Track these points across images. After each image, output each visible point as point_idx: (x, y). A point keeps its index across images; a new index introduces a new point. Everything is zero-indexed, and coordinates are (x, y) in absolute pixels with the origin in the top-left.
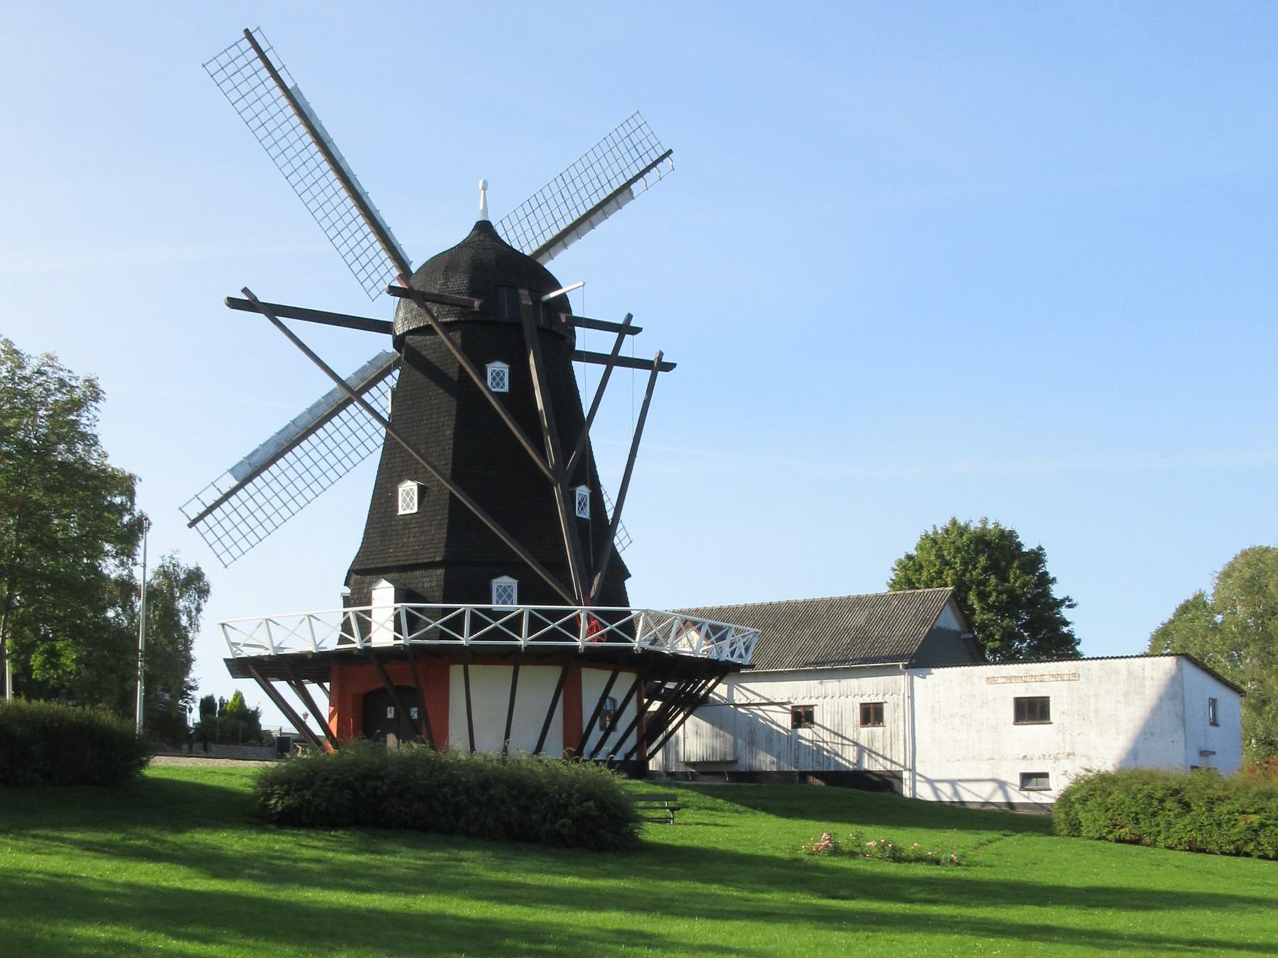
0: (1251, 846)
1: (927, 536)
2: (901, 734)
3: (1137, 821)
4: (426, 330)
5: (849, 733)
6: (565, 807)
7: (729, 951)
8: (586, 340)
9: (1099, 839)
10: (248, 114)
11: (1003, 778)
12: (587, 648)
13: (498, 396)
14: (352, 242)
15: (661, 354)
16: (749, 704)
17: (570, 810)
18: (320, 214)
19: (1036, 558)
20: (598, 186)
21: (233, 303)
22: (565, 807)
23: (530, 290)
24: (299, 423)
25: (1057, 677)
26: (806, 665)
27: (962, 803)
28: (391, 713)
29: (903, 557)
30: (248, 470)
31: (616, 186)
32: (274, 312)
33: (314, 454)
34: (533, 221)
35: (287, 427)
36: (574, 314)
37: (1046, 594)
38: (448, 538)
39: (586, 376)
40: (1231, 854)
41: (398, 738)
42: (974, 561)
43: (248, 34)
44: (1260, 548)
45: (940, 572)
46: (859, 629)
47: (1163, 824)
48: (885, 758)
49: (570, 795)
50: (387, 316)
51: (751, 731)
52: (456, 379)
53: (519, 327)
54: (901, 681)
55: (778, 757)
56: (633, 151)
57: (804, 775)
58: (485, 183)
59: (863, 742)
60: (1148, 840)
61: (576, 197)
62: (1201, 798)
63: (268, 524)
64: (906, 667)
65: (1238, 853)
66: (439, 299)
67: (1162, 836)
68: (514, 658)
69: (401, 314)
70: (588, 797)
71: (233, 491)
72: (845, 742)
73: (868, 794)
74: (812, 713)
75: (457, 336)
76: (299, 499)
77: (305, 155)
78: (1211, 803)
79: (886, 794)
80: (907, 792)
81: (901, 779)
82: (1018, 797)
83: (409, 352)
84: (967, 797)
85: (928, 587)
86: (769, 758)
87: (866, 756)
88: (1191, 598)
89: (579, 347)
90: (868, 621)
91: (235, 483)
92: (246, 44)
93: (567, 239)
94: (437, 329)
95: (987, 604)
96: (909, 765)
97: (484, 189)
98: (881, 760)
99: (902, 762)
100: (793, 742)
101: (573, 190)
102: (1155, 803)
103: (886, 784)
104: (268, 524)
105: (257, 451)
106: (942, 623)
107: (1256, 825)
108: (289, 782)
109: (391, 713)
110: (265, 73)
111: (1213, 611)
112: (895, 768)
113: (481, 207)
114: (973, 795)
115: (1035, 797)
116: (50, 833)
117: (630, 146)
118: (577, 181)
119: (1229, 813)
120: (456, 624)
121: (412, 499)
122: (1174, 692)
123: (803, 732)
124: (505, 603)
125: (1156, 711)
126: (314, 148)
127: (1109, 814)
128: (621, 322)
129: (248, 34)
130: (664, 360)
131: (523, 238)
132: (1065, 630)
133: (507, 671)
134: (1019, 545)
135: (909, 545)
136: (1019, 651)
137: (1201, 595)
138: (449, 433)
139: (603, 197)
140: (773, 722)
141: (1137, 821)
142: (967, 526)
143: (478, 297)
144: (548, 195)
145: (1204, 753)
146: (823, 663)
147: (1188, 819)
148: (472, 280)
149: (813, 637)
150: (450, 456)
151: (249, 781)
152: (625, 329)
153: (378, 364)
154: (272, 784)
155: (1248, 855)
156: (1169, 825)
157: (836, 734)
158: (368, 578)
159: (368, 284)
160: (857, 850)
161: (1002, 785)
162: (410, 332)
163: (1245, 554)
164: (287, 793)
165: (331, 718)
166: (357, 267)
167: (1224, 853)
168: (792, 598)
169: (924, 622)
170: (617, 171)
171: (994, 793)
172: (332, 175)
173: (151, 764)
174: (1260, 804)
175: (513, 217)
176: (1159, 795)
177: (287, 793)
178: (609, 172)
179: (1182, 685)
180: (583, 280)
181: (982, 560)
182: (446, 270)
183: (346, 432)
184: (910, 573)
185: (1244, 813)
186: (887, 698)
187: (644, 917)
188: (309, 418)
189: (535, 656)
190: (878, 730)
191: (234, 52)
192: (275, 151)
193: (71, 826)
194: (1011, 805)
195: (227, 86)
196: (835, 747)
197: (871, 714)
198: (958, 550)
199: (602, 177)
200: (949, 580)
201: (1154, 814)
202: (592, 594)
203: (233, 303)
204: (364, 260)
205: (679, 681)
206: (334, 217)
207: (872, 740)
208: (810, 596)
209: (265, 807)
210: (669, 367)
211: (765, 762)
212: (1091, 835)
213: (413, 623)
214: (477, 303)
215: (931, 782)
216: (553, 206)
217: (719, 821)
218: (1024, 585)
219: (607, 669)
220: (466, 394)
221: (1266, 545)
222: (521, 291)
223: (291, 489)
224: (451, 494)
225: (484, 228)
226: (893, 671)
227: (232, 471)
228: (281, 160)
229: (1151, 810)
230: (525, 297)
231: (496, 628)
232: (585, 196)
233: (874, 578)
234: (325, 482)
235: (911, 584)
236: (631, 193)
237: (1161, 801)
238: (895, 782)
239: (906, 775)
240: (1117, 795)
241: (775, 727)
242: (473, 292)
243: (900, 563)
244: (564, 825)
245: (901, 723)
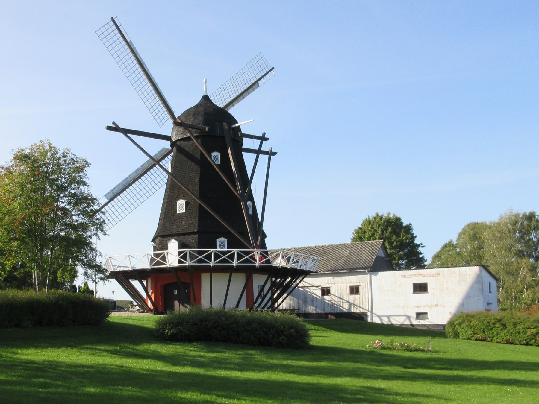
0: (533, 341)
1: (366, 220)
2: (367, 298)
3: (484, 332)
6: (283, 332)
8: (247, 143)
9: (468, 339)
10: (113, 52)
11: (409, 315)
12: (260, 266)
13: (217, 165)
14: (152, 104)
15: (272, 149)
17: (285, 333)
19: (408, 228)
20: (246, 82)
21: (109, 128)
22: (283, 332)
23: (227, 123)
24: (132, 177)
25: (431, 275)
26: (327, 271)
27: (392, 324)
28: (176, 293)
29: (357, 228)
30: (112, 195)
31: (253, 82)
32: (126, 132)
35: (127, 178)
36: (243, 132)
37: (413, 243)
38: (199, 222)
39: (248, 159)
40: (524, 344)
41: (180, 303)
42: (387, 230)
43: (113, 20)
44: (474, 223)
45: (373, 234)
46: (347, 257)
47: (495, 333)
48: (360, 307)
50: (169, 134)
51: (306, 298)
52: (199, 159)
53: (223, 137)
54: (367, 277)
55: (316, 307)
56: (259, 68)
57: (327, 315)
58: (206, 80)
59: (351, 301)
60: (489, 339)
61: (238, 86)
63: (120, 217)
64: (368, 271)
65: (527, 344)
66: (192, 127)
67: (495, 338)
68: (231, 270)
69: (175, 133)
70: (291, 327)
71: (106, 204)
73: (354, 322)
74: (329, 290)
75: (199, 141)
77: (134, 69)
78: (515, 324)
80: (369, 320)
81: (367, 316)
82: (415, 322)
83: (178, 147)
84: (394, 322)
85: (368, 240)
86: (312, 308)
88: (447, 242)
89: (244, 146)
90: (350, 253)
91: (107, 201)
92: (112, 23)
93: (234, 103)
94: (193, 138)
95: (393, 246)
96: (370, 310)
97: (206, 82)
98: (359, 308)
99: (367, 309)
100: (322, 301)
102: (492, 325)
103: (361, 317)
104: (120, 217)
105: (115, 188)
107: (535, 333)
108: (172, 323)
109: (176, 293)
111: (455, 247)
112: (364, 311)
113: (204, 90)
114: (397, 321)
115: (422, 322)
116: (89, 346)
117: (258, 65)
119: (523, 328)
120: (209, 257)
121: (183, 207)
123: (326, 297)
124: (222, 248)
125: (472, 288)
127: (472, 330)
128: (261, 135)
129: (113, 20)
131: (219, 102)
132: (421, 256)
134: (402, 223)
137: (452, 241)
140: (314, 294)
141: (484, 332)
142: (382, 216)
143: (207, 126)
144: (228, 85)
145: (488, 304)
146: (334, 270)
147: (506, 331)
149: (328, 260)
150: (198, 190)
152: (263, 139)
154: (165, 324)
155: (531, 345)
156: (498, 333)
158: (165, 239)
159: (159, 121)
160: (391, 347)
161: (408, 317)
162: (176, 141)
163: (469, 225)
164: (172, 328)
165: (152, 294)
166: (154, 114)
167: (521, 344)
169: (373, 254)
171: (405, 321)
176: (493, 321)
180: (245, 118)
181: (390, 229)
182: (194, 115)
184: (361, 235)
185: (529, 328)
187: (296, 375)
188: (135, 175)
189: (238, 269)
190: (357, 296)
191: (107, 27)
193: (84, 344)
194: (412, 325)
196: (339, 303)
197: (355, 290)
198: (379, 226)
201: (491, 329)
203: (109, 128)
204: (157, 111)
205: (285, 278)
206: (145, 93)
207: (355, 300)
209: (163, 334)
210: (275, 154)
211: (311, 309)
212: (463, 338)
214: (207, 128)
215: (379, 317)
216: (229, 90)
217: (322, 335)
218: (407, 239)
220: (204, 165)
221: (476, 222)
222: (224, 123)
224: (200, 204)
225: (206, 98)
226: (364, 273)
227: (106, 196)
229: (490, 328)
230: (226, 127)
232: (241, 86)
233: (345, 236)
235: (361, 239)
236: (258, 84)
237: (494, 324)
238: (365, 316)
239: (369, 314)
240: (474, 322)
241: (314, 296)
242: (206, 124)
243: (355, 230)
244: (282, 339)
245: (367, 294)
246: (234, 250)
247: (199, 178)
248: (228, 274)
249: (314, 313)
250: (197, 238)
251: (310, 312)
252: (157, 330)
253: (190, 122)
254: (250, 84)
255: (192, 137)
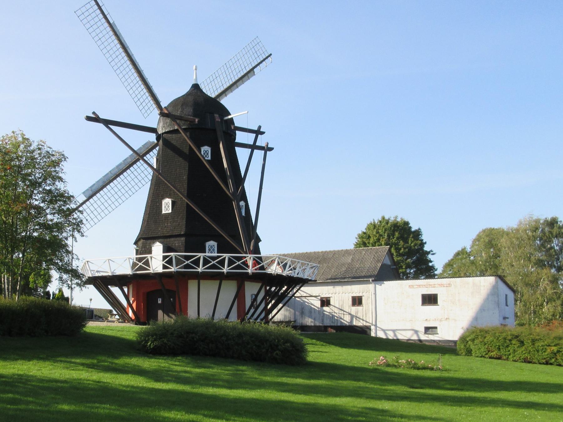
0: (553, 360)
1: (371, 224)
2: (370, 309)
3: (499, 349)
4: (175, 132)
5: (347, 309)
6: (277, 346)
7: (424, 418)
8: (241, 137)
9: (481, 357)
11: (416, 329)
12: (253, 273)
14: (137, 92)
15: (268, 144)
16: (301, 297)
17: (280, 347)
18: (123, 80)
19: (418, 233)
21: (89, 118)
22: (277, 346)
23: (219, 115)
24: (113, 172)
25: (441, 285)
26: (327, 280)
27: (398, 339)
28: (160, 301)
29: (360, 233)
30: (90, 193)
31: (248, 70)
32: (107, 123)
33: (119, 186)
34: (213, 85)
36: (236, 125)
39: (242, 154)
40: (544, 364)
41: (164, 312)
42: (393, 235)
45: (379, 240)
46: (349, 264)
47: (511, 351)
48: (363, 320)
49: (279, 341)
51: (304, 309)
52: (188, 153)
53: (215, 130)
54: (371, 286)
55: (315, 319)
57: (326, 328)
58: (196, 67)
62: (528, 339)
63: (99, 217)
64: (373, 281)
65: (547, 363)
66: (181, 118)
67: (511, 356)
68: (221, 277)
69: (161, 124)
70: (287, 341)
71: (84, 202)
72: (345, 313)
73: (356, 336)
74: (329, 300)
75: (188, 134)
76: (113, 206)
77: (117, 53)
78: (533, 341)
79: (364, 335)
80: (373, 334)
81: (370, 329)
82: (423, 337)
83: (165, 142)
84: (400, 337)
85: (373, 246)
86: (310, 320)
87: (354, 319)
88: (460, 250)
90: (352, 260)
91: (85, 199)
94: (181, 131)
95: (400, 253)
96: (374, 323)
97: (196, 69)
98: (361, 321)
99: (371, 322)
100: (321, 313)
101: (230, 71)
102: (508, 341)
103: (364, 331)
104: (99, 217)
105: (94, 185)
106: (385, 262)
107: (555, 351)
108: (156, 335)
109: (160, 301)
110: (101, 16)
111: (469, 255)
112: (367, 324)
113: (194, 78)
114: (403, 336)
115: (431, 337)
116: (63, 359)
117: (254, 52)
118: (232, 67)
121: (168, 207)
122: (494, 292)
123: (326, 308)
124: (211, 253)
125: (487, 300)
126: (121, 50)
128: (256, 129)
130: (269, 146)
131: (211, 90)
132: (430, 264)
133: (218, 282)
134: (410, 227)
135: (362, 228)
136: (410, 273)
137: (465, 248)
138: (185, 177)
139: (242, 74)
140: (312, 304)
141: (499, 349)
142: (389, 219)
145: (505, 318)
146: (335, 279)
147: (523, 348)
148: (194, 110)
150: (186, 188)
151: (134, 334)
152: (258, 132)
153: (146, 147)
154: (148, 336)
155: (551, 364)
156: (514, 351)
157: (340, 309)
158: (149, 241)
159: (143, 111)
160: (396, 364)
161: (416, 332)
162: (165, 133)
163: (484, 231)
164: (155, 340)
165: (133, 302)
166: (139, 103)
167: (540, 363)
168: (316, 250)
169: (378, 261)
170: (249, 63)
171: (412, 336)
172: (129, 62)
173: (87, 325)
174: (557, 342)
175: (205, 82)
176: (510, 337)
177: (155, 340)
178: (245, 63)
179: (497, 288)
180: (240, 110)
183: (133, 177)
184: (365, 240)
185: (549, 346)
186: (364, 294)
187: (291, 394)
188: (117, 170)
189: (229, 276)
190: (360, 308)
191: (88, 6)
192: (105, 51)
193: (58, 356)
194: (420, 341)
195: (85, 21)
196: (340, 315)
197: (357, 301)
198: (385, 230)
199: (242, 65)
200: (383, 243)
201: (507, 346)
202: (251, 248)
203: (89, 118)
204: (141, 100)
205: (280, 286)
206: (129, 81)
207: (357, 312)
208: (324, 250)
209: (145, 346)
211: (309, 321)
213: (170, 262)
214: (197, 120)
215: (384, 331)
216: (222, 78)
217: (320, 350)
218: (415, 245)
219: (258, 282)
220: (194, 160)
221: (492, 227)
222: (215, 115)
223: (109, 201)
224: (187, 204)
225: (196, 87)
226: (367, 282)
227: (84, 193)
228: (108, 55)
229: (506, 344)
231: (214, 264)
232: (235, 74)
233: (348, 242)
234: (124, 199)
235: (365, 244)
236: (254, 72)
237: (510, 340)
240: (489, 338)
241: (313, 306)
242: (195, 115)
243: (359, 235)
244: (277, 354)
246: (225, 255)
247: (187, 175)
248: (218, 282)
249: (311, 326)
250: (184, 241)
251: (308, 324)
252: (139, 343)
253: (178, 113)
254: (245, 72)
255: (180, 130)
